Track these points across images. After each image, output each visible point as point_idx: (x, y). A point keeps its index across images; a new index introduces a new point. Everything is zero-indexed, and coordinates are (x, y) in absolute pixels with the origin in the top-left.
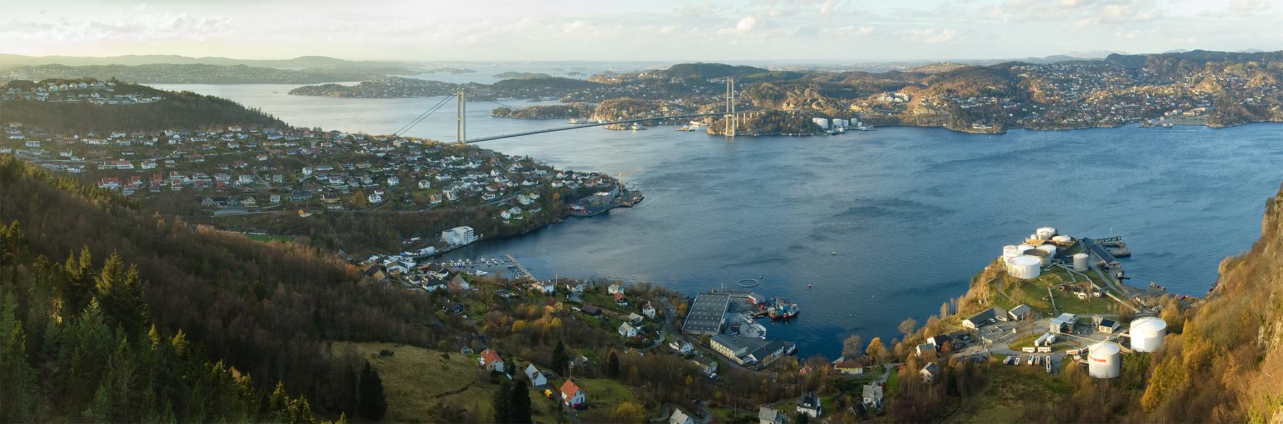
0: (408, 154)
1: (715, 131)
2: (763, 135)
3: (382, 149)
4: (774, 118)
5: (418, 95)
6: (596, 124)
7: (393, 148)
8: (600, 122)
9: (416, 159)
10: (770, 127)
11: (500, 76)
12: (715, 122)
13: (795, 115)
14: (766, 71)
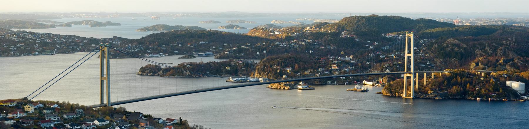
0: (43, 120)
1: (391, 92)
2: (447, 98)
3: (10, 115)
4: (459, 79)
5: (52, 53)
6: (257, 83)
7: (25, 114)
8: (261, 80)
9: (52, 125)
10: (454, 89)
11: (147, 29)
12: (392, 83)
13: (485, 77)
14: (451, 25)
